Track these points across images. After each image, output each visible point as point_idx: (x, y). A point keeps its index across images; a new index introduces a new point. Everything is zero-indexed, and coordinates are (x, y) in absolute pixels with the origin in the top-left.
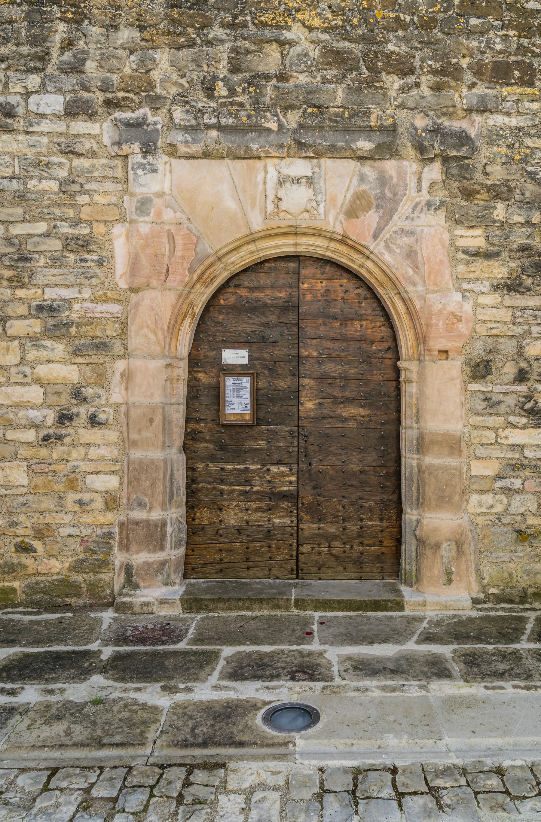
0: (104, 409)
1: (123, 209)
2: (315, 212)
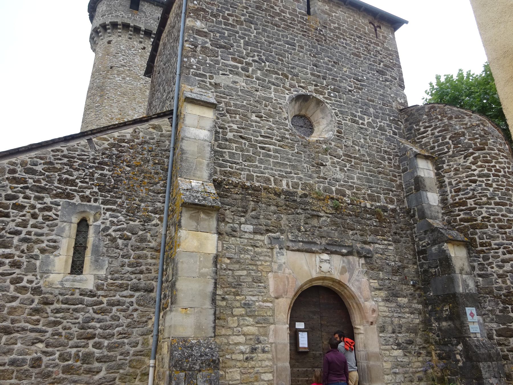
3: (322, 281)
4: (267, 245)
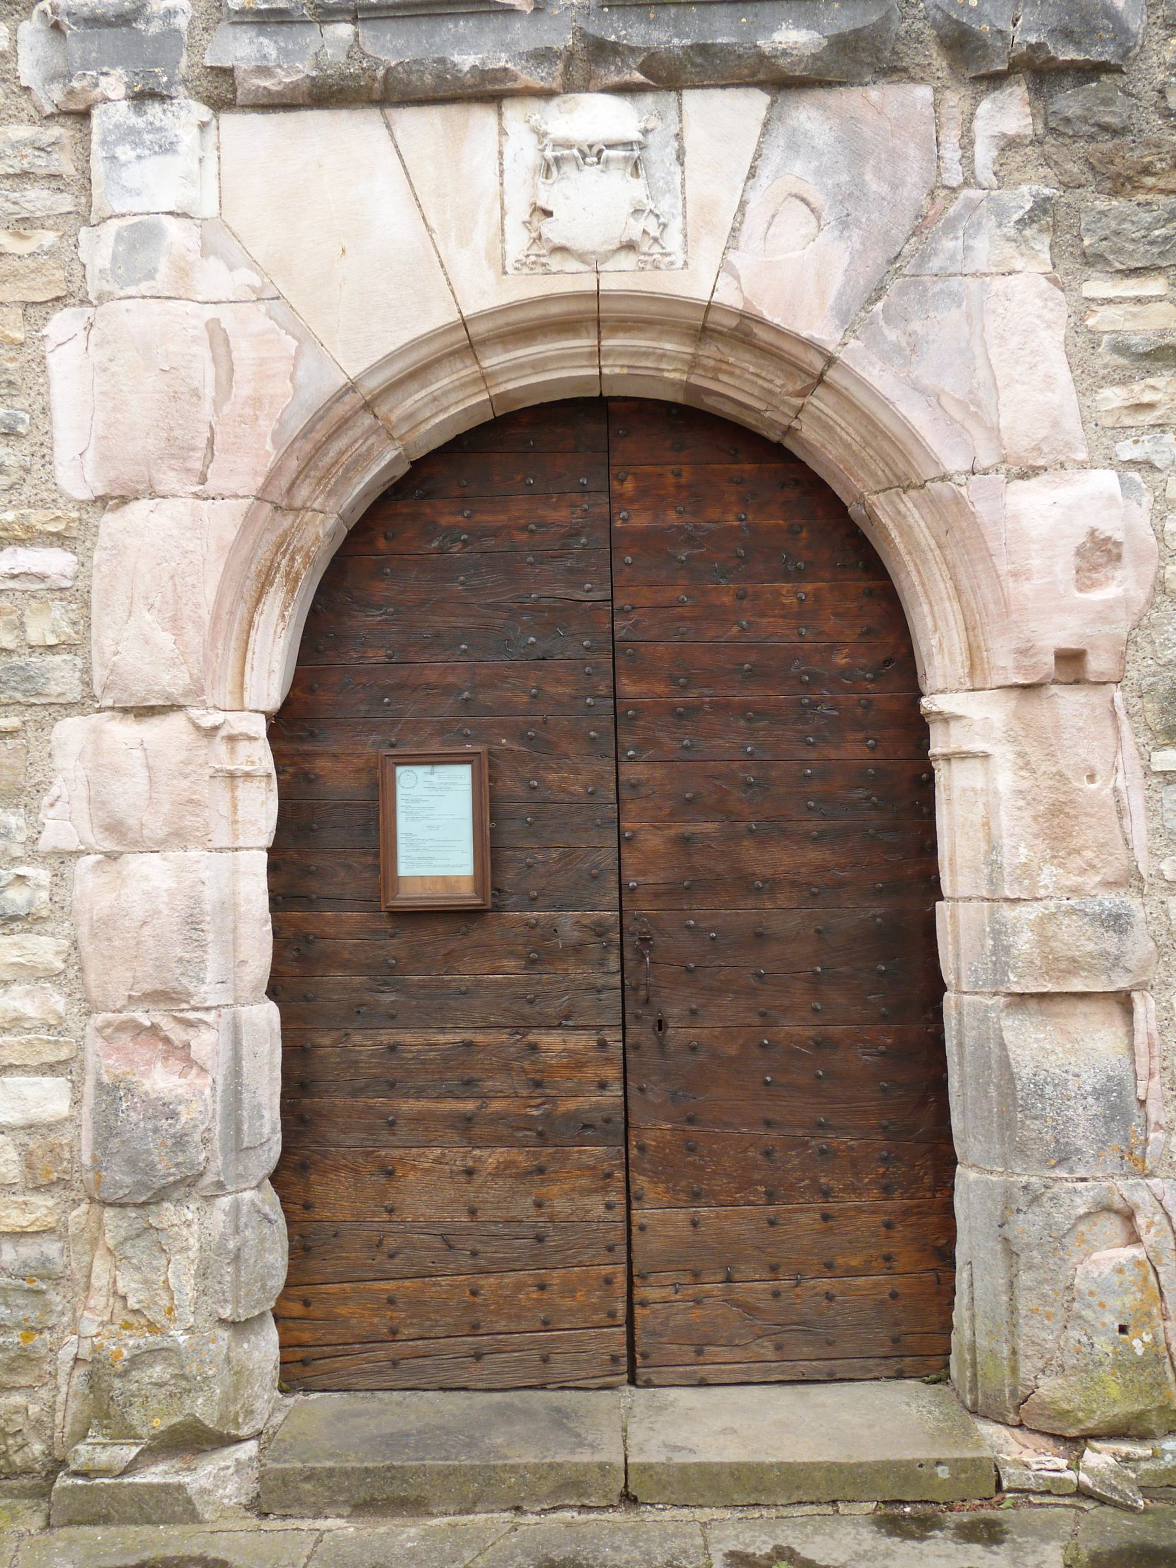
0: (22, 870)
1: (76, 266)
2: (656, 249)
3: (584, 343)
4: (38, 93)
